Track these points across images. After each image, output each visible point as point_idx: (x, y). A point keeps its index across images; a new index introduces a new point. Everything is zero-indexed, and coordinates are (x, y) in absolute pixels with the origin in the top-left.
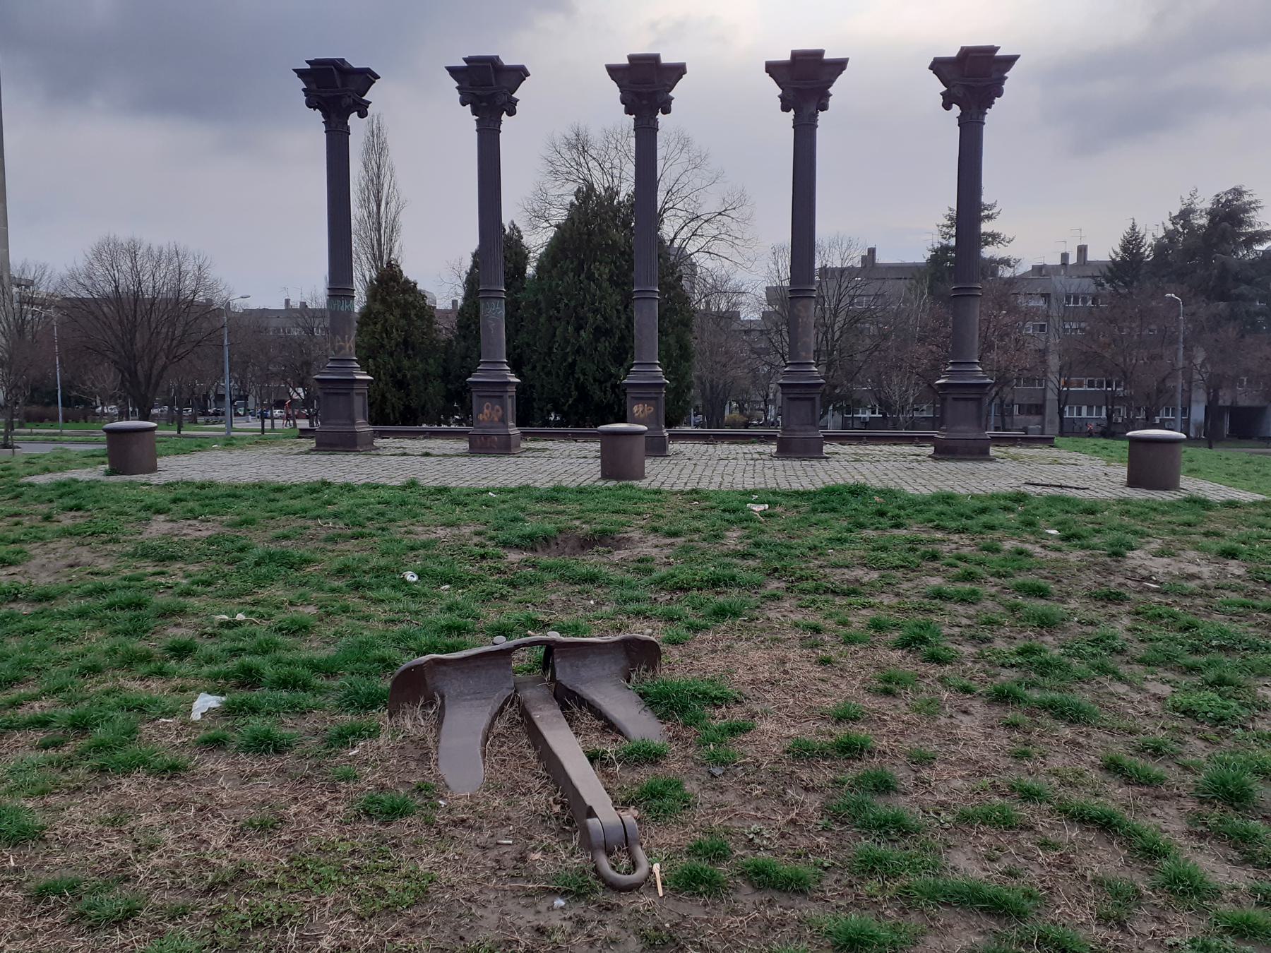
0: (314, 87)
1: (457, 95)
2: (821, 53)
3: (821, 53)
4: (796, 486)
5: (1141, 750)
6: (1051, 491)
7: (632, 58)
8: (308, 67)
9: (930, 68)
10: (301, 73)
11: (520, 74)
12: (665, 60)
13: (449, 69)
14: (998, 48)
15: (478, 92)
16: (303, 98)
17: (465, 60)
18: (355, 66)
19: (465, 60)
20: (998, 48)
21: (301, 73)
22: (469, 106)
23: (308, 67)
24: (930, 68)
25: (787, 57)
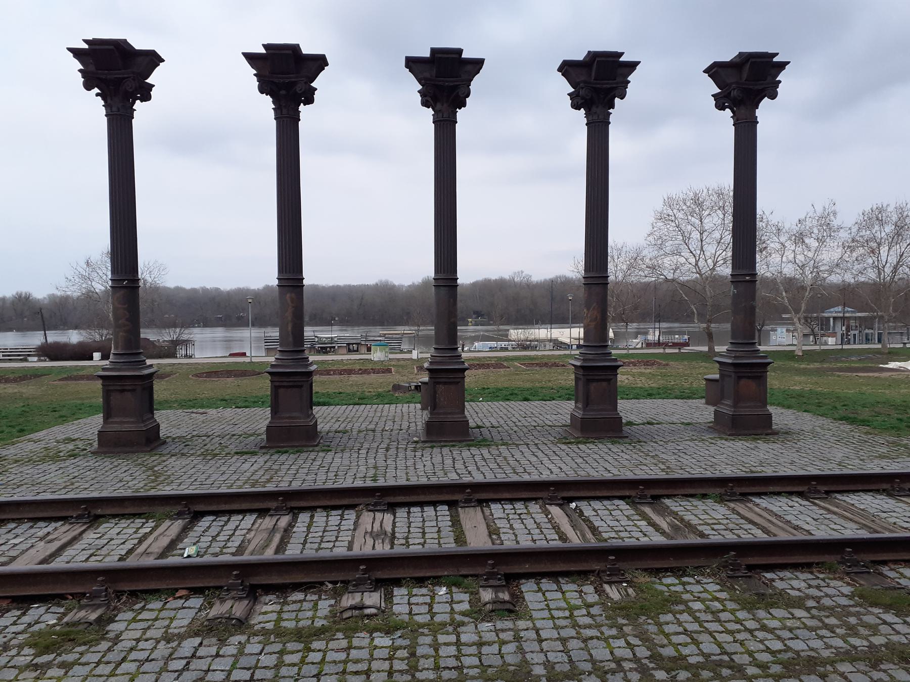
0: (92, 68)
1: (255, 83)
2: (460, 51)
3: (460, 51)
4: (478, 478)
5: (120, 560)
6: (822, 504)
7: (434, 51)
8: (86, 46)
9: (559, 70)
10: (77, 53)
11: (152, 59)
12: (306, 50)
13: (245, 54)
14: (622, 54)
15: (276, 80)
16: (419, 98)
17: (264, 46)
18: (137, 48)
19: (264, 46)
20: (622, 54)
21: (77, 53)
22: (582, 111)
23: (86, 46)
24: (559, 70)
25: (427, 54)
